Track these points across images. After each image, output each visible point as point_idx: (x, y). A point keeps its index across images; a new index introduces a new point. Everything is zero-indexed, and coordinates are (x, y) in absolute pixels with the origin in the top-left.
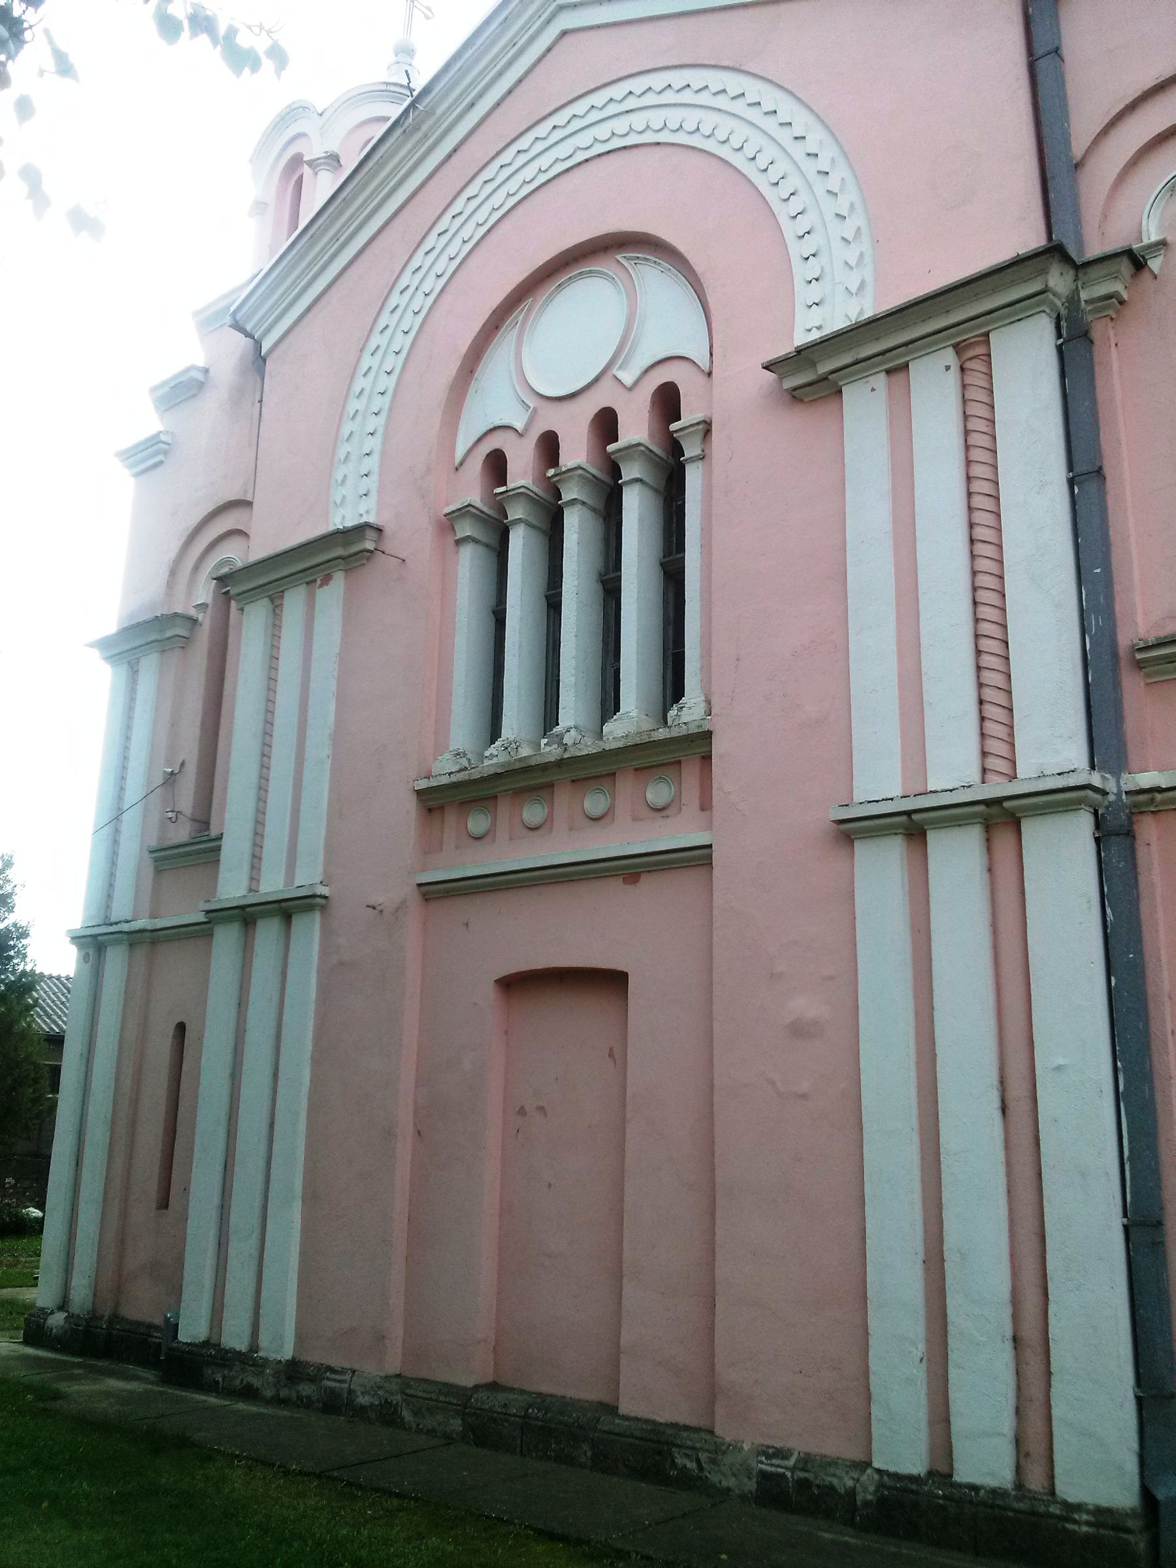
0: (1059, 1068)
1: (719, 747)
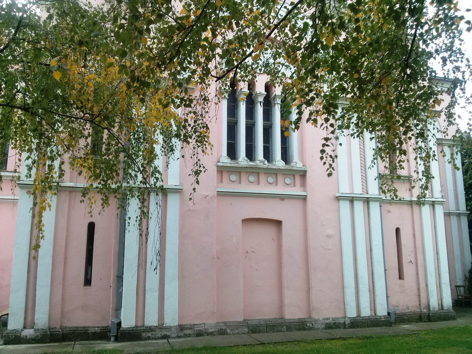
0: (376, 245)
1: (308, 174)
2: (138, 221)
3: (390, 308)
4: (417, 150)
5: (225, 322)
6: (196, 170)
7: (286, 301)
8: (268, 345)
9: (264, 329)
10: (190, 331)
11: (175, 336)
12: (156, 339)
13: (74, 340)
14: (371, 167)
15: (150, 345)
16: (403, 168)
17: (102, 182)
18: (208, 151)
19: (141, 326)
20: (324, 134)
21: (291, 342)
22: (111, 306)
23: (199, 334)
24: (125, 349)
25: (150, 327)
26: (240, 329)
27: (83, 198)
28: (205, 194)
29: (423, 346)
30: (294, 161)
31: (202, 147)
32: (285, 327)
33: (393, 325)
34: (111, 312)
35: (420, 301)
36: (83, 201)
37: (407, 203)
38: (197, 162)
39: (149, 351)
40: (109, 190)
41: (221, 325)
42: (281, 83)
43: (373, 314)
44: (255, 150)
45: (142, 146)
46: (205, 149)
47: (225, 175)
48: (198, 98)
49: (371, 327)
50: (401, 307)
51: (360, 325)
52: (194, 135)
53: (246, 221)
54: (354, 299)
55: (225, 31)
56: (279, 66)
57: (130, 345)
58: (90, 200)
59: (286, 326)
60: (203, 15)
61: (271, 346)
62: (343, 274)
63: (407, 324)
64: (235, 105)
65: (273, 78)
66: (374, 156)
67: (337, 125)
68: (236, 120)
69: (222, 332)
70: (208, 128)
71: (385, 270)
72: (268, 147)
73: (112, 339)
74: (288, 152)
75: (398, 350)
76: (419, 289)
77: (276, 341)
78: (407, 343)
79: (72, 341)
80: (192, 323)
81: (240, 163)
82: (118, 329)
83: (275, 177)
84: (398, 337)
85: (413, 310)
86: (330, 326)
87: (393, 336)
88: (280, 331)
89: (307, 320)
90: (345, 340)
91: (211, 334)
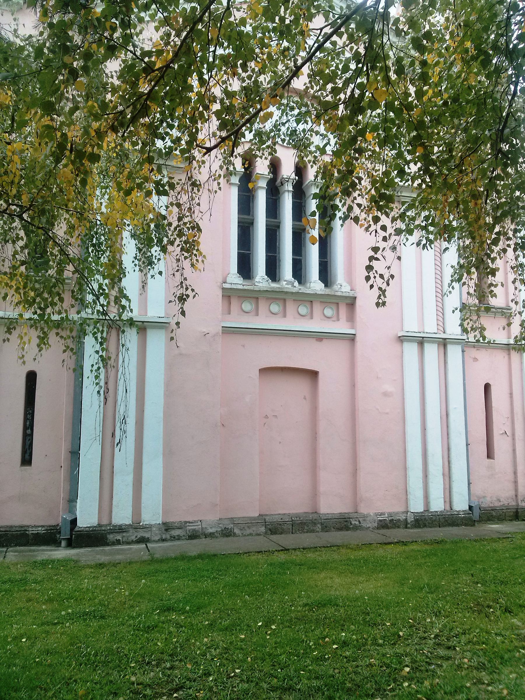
0: (455, 408)
1: (358, 303)
2: (94, 372)
3: (472, 499)
4: (516, 269)
5: (232, 518)
6: (180, 294)
7: (322, 488)
8: (293, 552)
9: (289, 529)
10: (180, 531)
11: (158, 538)
12: (128, 543)
13: (7, 546)
14: (448, 293)
15: (118, 552)
16: (495, 295)
17: (39, 312)
18: (200, 265)
19: (106, 525)
20: (371, 240)
21: (327, 547)
22: (63, 495)
23: (193, 536)
24: (81, 559)
25: (120, 526)
26: (254, 529)
27: (7, 335)
28: (204, 330)
29: (517, 556)
30: (338, 282)
31: (191, 260)
32: (319, 526)
33: (476, 524)
34: (62, 504)
35: (516, 490)
36: (8, 340)
37: (502, 347)
38: (182, 283)
39: (117, 562)
40: (48, 323)
41: (226, 522)
42: (314, 162)
43: (448, 508)
44: (279, 265)
45: (104, 255)
46: (195, 262)
47: (235, 303)
48: (183, 181)
49: (444, 526)
50: (488, 499)
51: (429, 523)
52: (178, 240)
53: (265, 371)
54: (421, 485)
55: (228, 78)
56: (311, 135)
57: (90, 552)
58: (22, 338)
59: (322, 524)
60: (183, 49)
61: (298, 553)
62: (405, 450)
63: (498, 524)
64: (249, 196)
65: (302, 154)
66: (452, 276)
67: (394, 228)
68: (251, 218)
69: (227, 533)
70: (200, 230)
71: (467, 445)
72: (300, 261)
73: (63, 543)
74: (329, 268)
75: (482, 561)
76: (515, 473)
77: (305, 546)
78: (495, 551)
79: (3, 547)
80: (183, 520)
81: (256, 284)
82: (72, 529)
83: (309, 306)
84: (483, 542)
85: (506, 503)
86: (383, 525)
87: (476, 541)
88: (313, 531)
89: (351, 516)
90: (405, 545)
91: (211, 535)
